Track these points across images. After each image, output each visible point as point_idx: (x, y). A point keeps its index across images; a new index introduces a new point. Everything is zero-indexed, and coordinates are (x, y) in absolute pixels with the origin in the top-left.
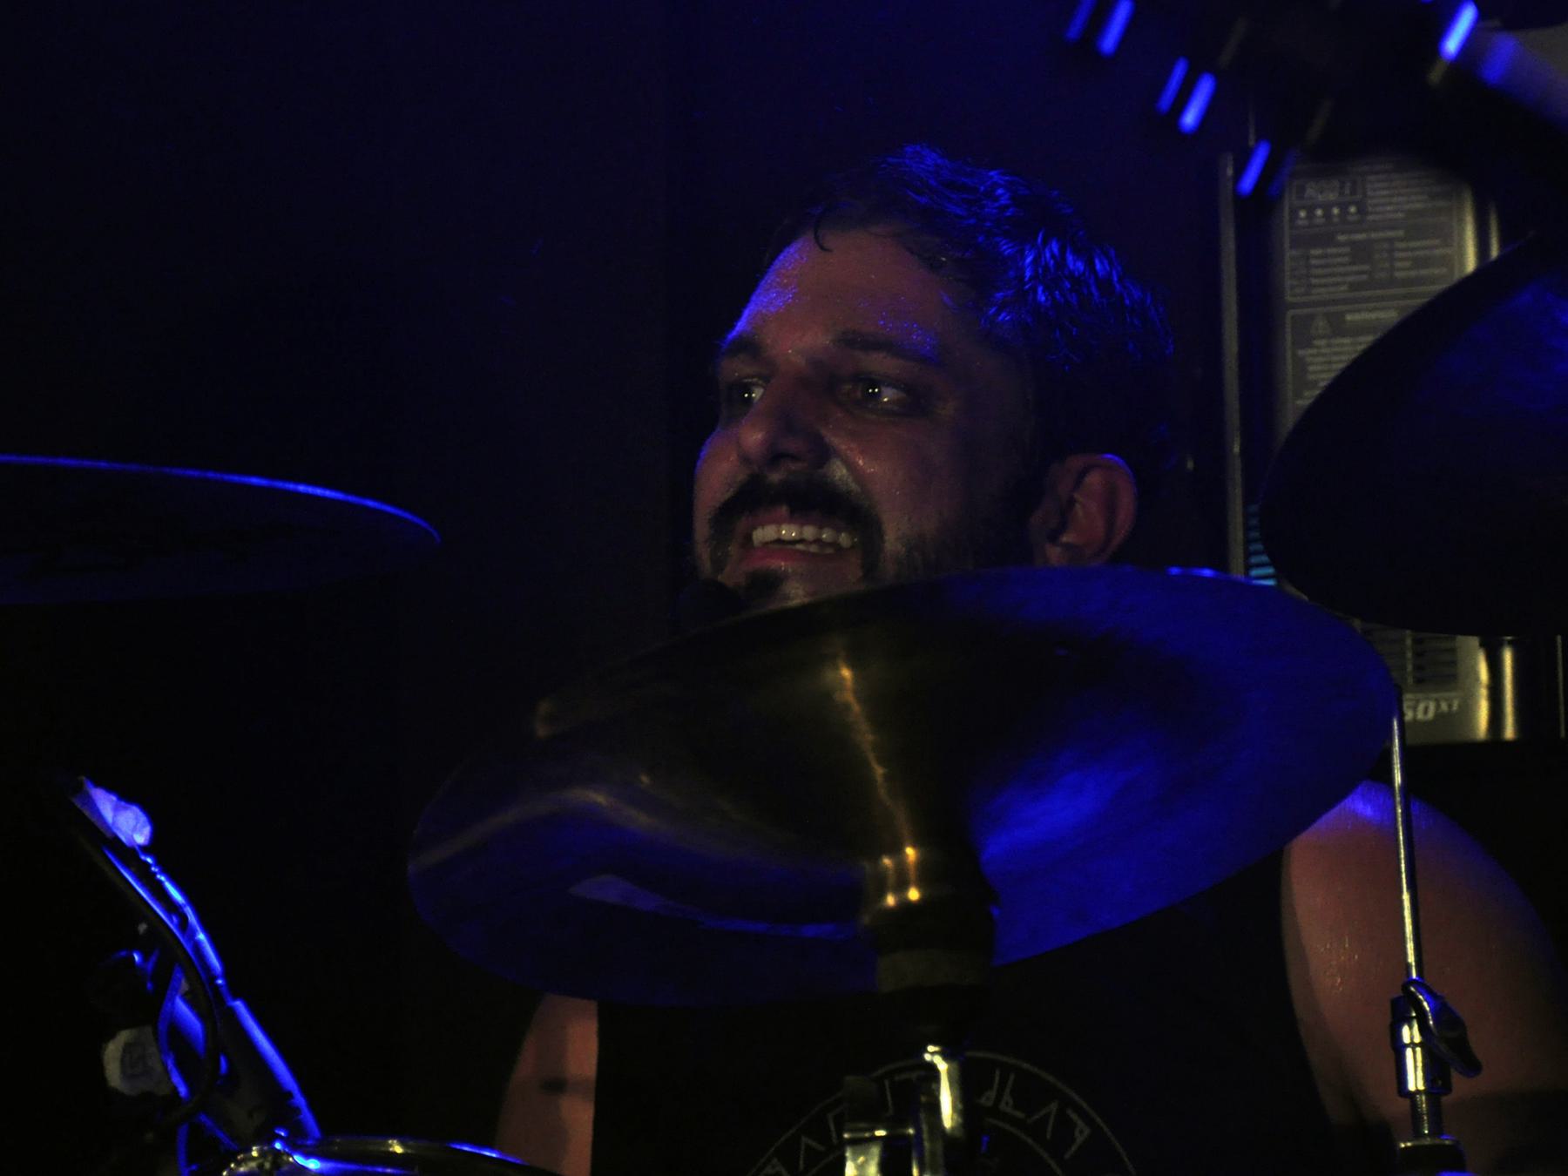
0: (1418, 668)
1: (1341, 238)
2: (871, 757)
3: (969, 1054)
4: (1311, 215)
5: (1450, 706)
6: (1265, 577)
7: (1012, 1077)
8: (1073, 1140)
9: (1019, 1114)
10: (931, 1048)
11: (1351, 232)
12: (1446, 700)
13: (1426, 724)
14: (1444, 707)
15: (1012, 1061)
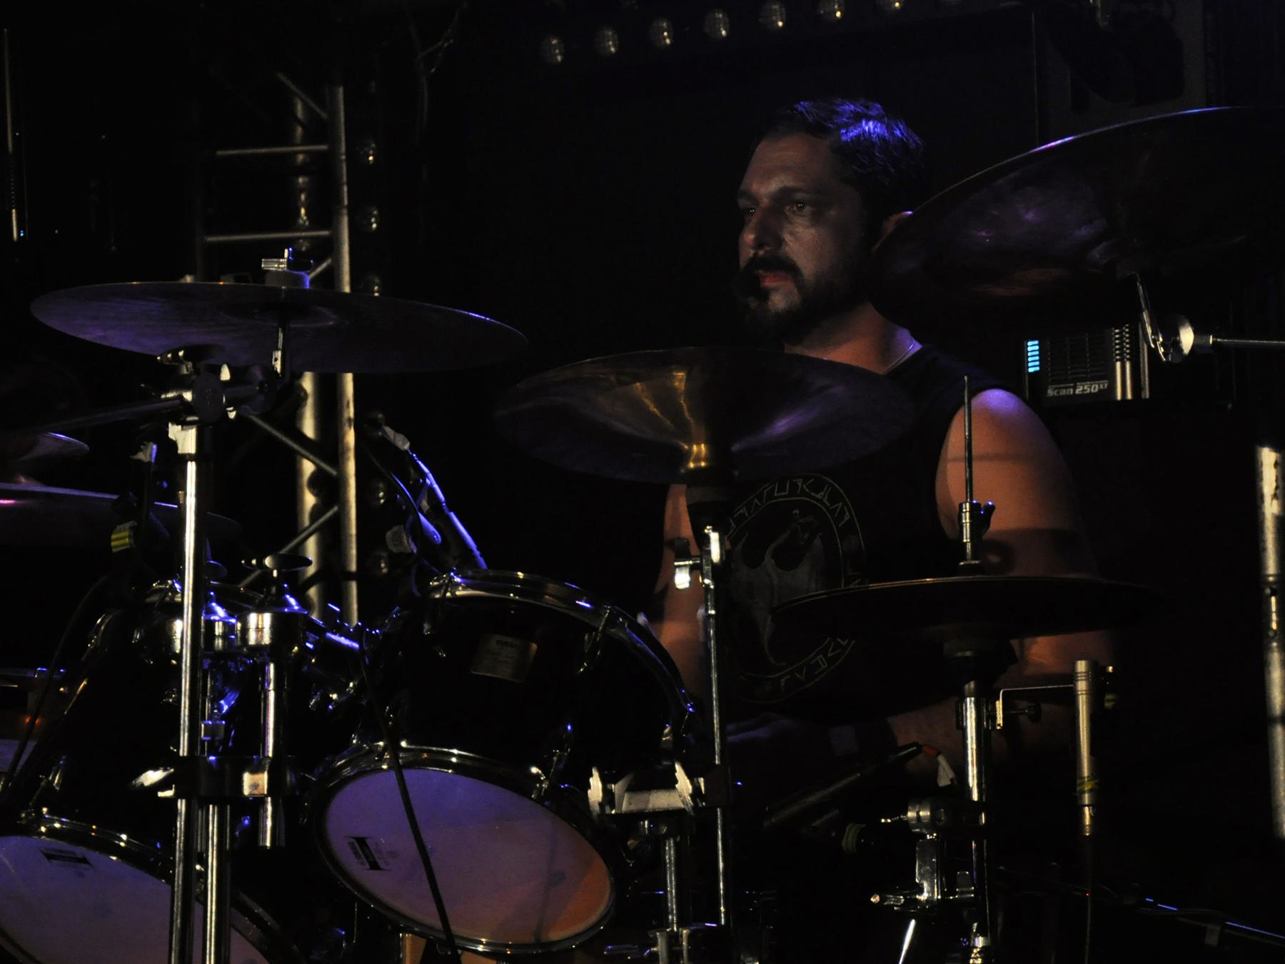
3: (269, 799)
5: (1104, 386)
6: (782, 684)
8: (843, 519)
9: (828, 504)
10: (708, 527)
13: (1094, 394)
14: (1102, 387)
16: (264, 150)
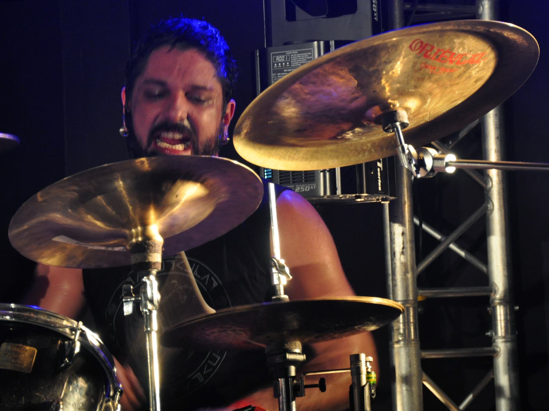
0: (305, 178)
1: (285, 71)
2: (128, 204)
4: (278, 65)
5: (313, 187)
7: (198, 266)
11: (287, 69)
12: (312, 186)
13: (308, 192)
15: (199, 262)
16: (264, 18)
